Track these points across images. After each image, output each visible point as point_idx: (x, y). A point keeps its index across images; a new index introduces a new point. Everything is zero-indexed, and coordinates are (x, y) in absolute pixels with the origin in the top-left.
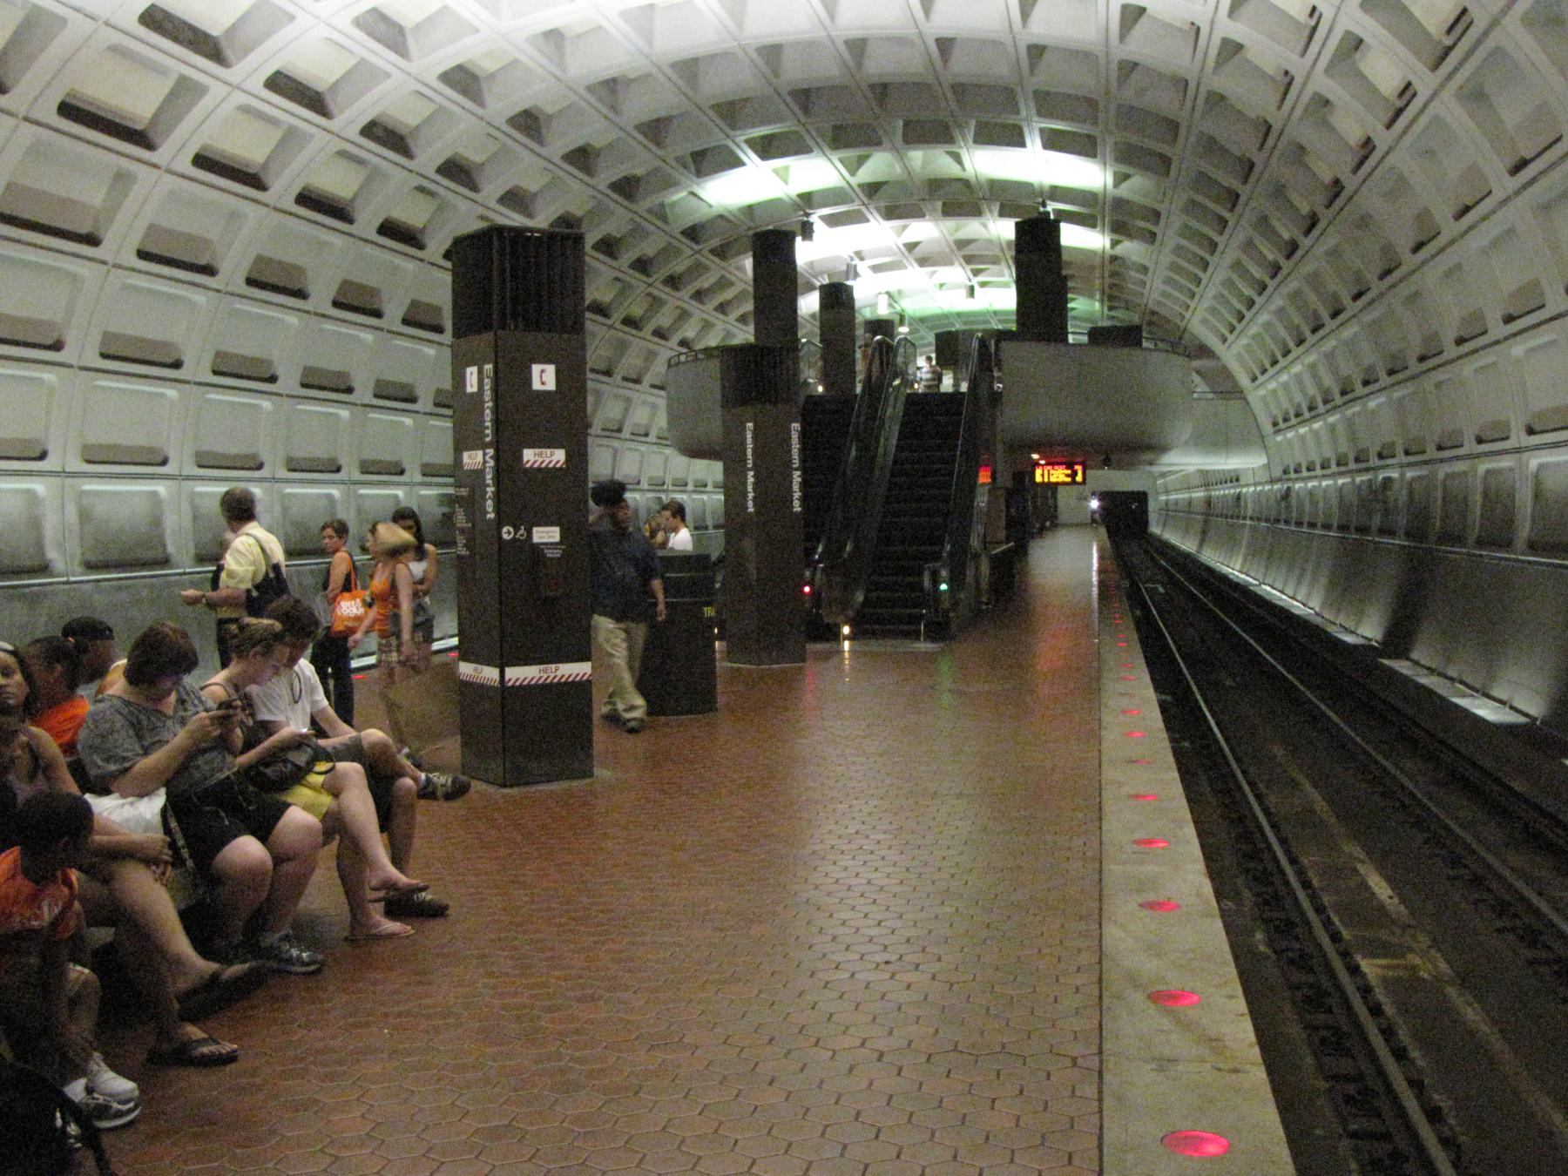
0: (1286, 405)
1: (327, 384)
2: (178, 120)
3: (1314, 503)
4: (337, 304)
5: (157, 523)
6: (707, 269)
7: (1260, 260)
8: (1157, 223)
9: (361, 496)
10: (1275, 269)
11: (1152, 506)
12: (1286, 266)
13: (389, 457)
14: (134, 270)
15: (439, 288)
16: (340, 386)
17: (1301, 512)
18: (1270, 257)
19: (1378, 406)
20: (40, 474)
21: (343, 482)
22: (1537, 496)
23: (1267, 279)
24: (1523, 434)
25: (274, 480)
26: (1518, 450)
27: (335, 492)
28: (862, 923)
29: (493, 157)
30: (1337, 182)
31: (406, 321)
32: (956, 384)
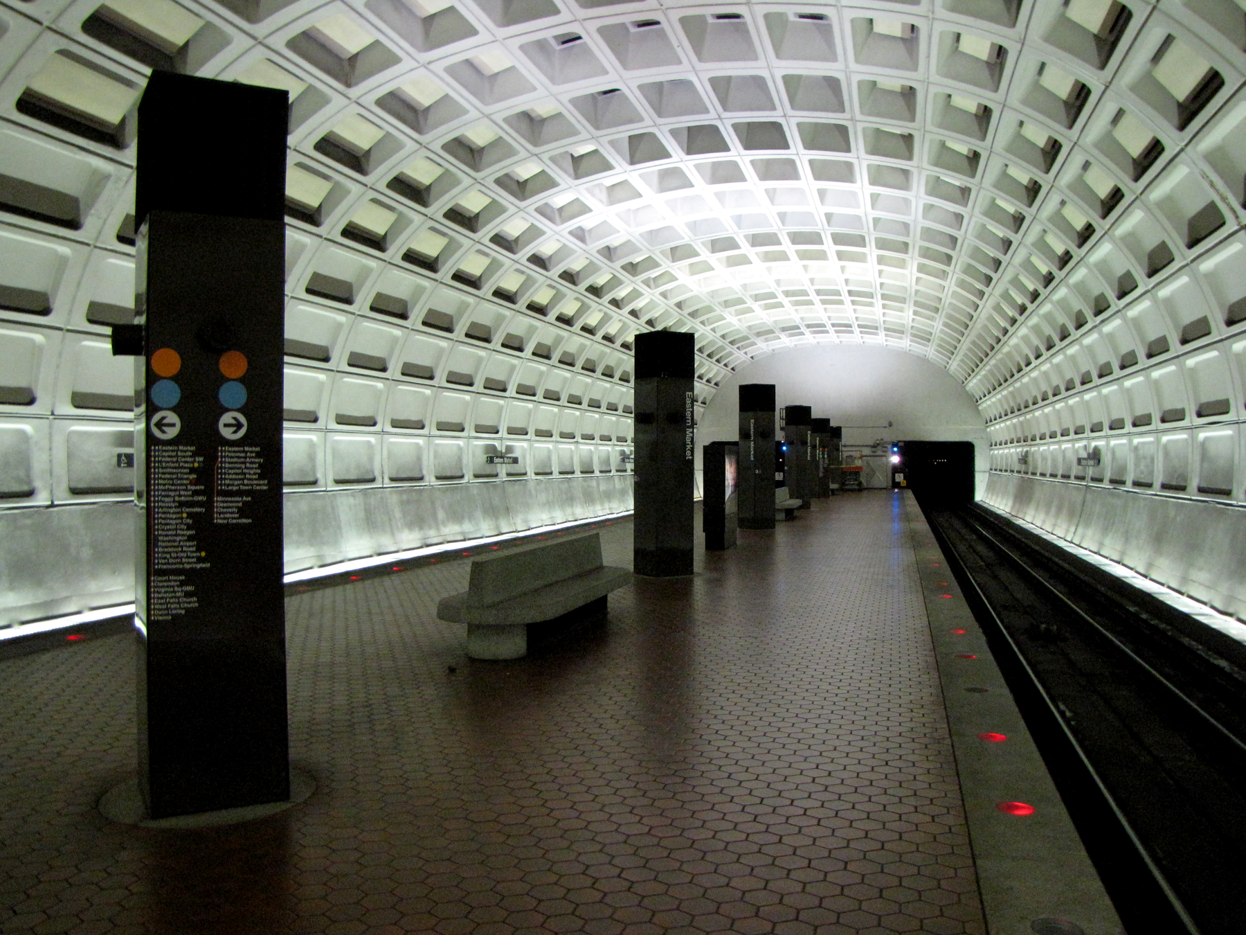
0: (1006, 407)
1: (415, 372)
2: (493, 274)
3: (1054, 461)
4: (372, 309)
5: (419, 459)
6: (642, 295)
7: (1011, 302)
8: (949, 264)
9: (438, 445)
10: (1023, 309)
11: (981, 464)
12: (1030, 307)
13: (414, 418)
14: (116, 252)
15: (628, 362)
16: (426, 374)
17: (1055, 466)
18: (1020, 302)
19: (1092, 398)
20: (316, 430)
21: (320, 430)
22: (1114, 458)
23: (1017, 316)
24: (1194, 416)
25: (470, 438)
26: (1157, 431)
27: (27, 427)
28: (742, 713)
29: (439, 179)
30: (1067, 253)
31: (534, 354)
32: (894, 453)
